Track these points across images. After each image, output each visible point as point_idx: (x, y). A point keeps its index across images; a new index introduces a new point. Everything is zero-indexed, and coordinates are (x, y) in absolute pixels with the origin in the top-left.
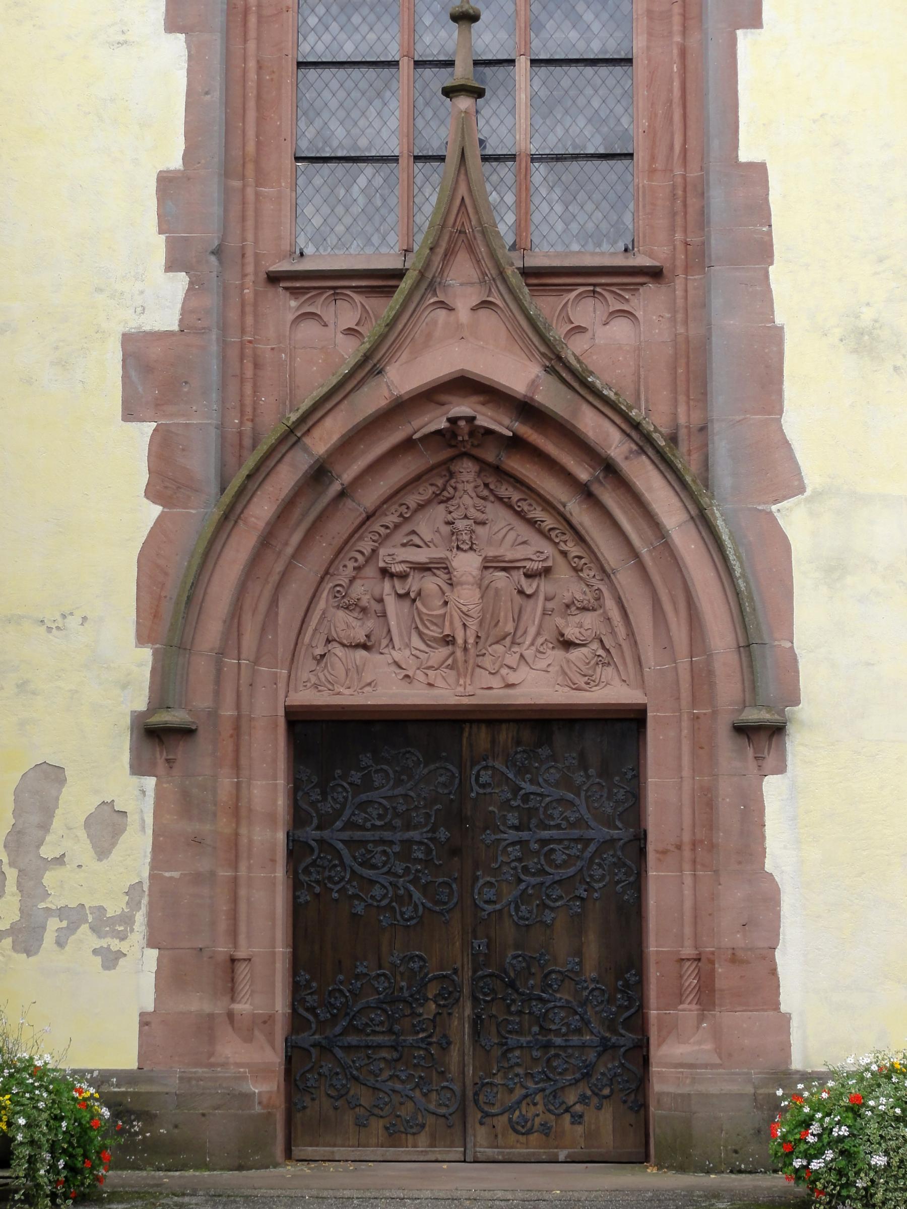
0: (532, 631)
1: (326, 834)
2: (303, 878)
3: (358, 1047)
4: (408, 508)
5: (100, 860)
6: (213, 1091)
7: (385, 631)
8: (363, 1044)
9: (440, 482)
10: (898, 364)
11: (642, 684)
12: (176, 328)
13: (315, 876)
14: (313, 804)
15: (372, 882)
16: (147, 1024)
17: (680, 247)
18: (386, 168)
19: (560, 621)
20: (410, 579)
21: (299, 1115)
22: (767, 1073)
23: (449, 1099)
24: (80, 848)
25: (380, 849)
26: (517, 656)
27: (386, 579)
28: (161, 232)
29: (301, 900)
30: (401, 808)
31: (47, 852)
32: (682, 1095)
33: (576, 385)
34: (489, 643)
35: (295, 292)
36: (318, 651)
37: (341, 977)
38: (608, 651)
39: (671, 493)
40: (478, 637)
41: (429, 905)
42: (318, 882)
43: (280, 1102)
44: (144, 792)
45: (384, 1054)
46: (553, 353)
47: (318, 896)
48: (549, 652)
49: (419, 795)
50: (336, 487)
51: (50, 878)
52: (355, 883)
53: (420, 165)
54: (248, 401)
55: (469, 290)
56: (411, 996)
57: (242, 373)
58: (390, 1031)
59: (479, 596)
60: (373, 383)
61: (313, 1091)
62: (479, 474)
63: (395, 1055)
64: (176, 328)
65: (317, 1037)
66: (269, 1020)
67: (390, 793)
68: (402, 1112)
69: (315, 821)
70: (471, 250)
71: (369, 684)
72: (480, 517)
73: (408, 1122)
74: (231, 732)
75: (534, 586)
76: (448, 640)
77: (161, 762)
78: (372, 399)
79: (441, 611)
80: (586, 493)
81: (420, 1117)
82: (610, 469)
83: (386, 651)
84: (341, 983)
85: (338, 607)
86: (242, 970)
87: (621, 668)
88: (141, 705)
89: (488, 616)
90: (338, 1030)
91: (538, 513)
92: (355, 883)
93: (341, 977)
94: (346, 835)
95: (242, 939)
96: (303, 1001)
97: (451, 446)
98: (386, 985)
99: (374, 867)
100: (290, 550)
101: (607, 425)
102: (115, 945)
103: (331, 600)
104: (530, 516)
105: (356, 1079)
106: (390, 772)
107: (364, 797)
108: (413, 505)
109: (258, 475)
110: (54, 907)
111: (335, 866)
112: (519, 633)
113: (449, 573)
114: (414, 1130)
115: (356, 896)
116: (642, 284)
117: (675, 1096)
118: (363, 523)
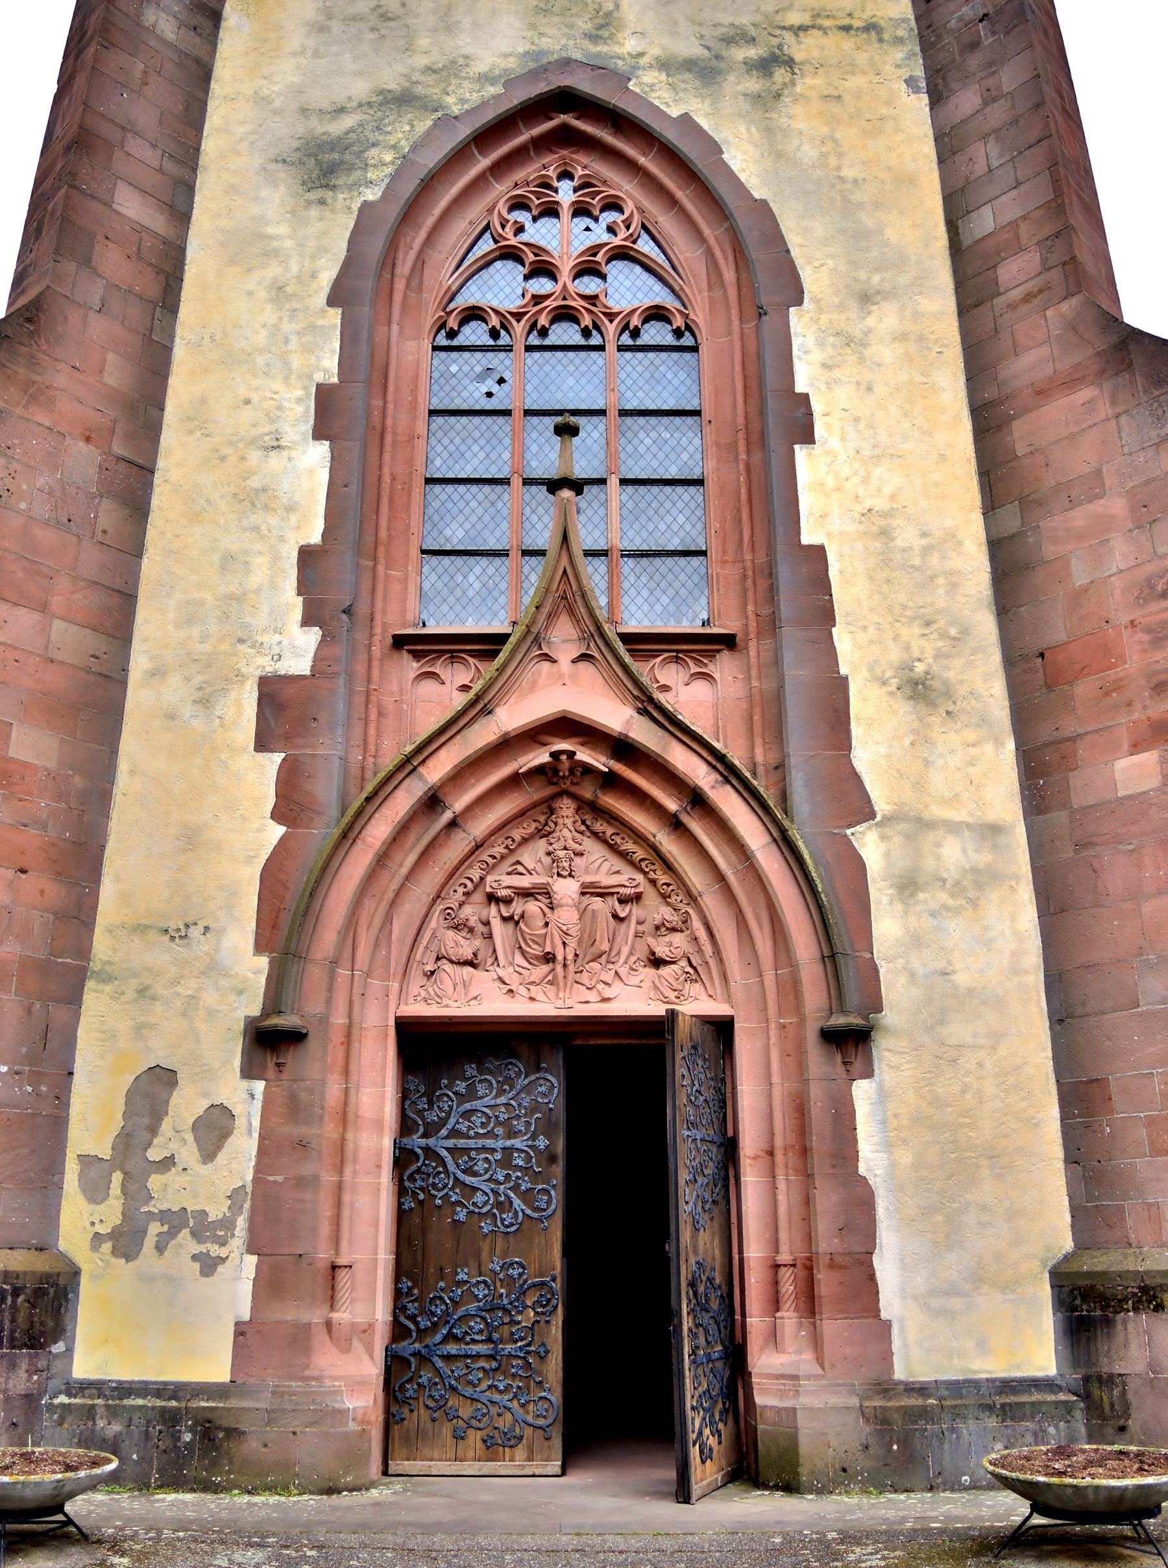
0: (625, 950)
1: (431, 1142)
2: (407, 1184)
3: (456, 1357)
4: (513, 841)
5: (205, 1163)
6: (306, 1407)
7: (491, 951)
8: (462, 1353)
9: (542, 819)
10: (950, 709)
11: (729, 999)
12: (308, 673)
13: (419, 1183)
14: (420, 1113)
15: (475, 1189)
16: (242, 1334)
17: (751, 616)
18: (497, 561)
19: (651, 941)
20: (515, 902)
21: (396, 1427)
22: (870, 1384)
23: (547, 1411)
24: (188, 1153)
25: (483, 1156)
26: (613, 972)
27: (493, 904)
28: (299, 594)
29: (406, 1207)
30: (503, 1117)
31: (154, 1155)
32: (785, 1409)
33: (666, 724)
34: (588, 958)
35: (417, 655)
36: (429, 968)
37: (442, 1284)
38: (695, 969)
39: (754, 818)
40: (576, 955)
41: (528, 1212)
42: (422, 1189)
43: (377, 1416)
44: (252, 1096)
45: (482, 1363)
46: (647, 696)
47: (421, 1203)
48: (641, 969)
49: (520, 1105)
50: (448, 816)
51: (155, 1182)
52: (457, 1190)
53: (527, 558)
54: (372, 740)
55: (570, 646)
56: (510, 1303)
57: (367, 716)
58: (489, 1340)
59: (577, 917)
60: (483, 721)
61: (411, 1402)
62: (577, 811)
63: (494, 1364)
64: (308, 673)
65: (417, 1345)
66: (369, 1329)
67: (493, 1102)
68: (500, 1423)
69: (421, 1129)
70: (572, 612)
71: (475, 998)
72: (578, 848)
73: (505, 1434)
74: (343, 1039)
75: (627, 910)
76: (549, 958)
77: (271, 1065)
78: (483, 735)
79: (544, 931)
80: (675, 824)
81: (517, 1430)
82: (697, 800)
83: (491, 968)
84: (442, 1290)
85: (448, 928)
86: (343, 1276)
87: (707, 985)
88: (255, 1010)
89: (586, 936)
90: (438, 1338)
91: (629, 846)
92: (457, 1190)
93: (442, 1284)
94: (450, 1143)
95: (344, 1244)
96: (404, 1308)
97: (553, 784)
98: (486, 1292)
99: (475, 1174)
100: (404, 870)
101: (695, 759)
102: (215, 1250)
103: (442, 921)
104: (623, 848)
105: (453, 1389)
106: (494, 1082)
107: (468, 1106)
108: (518, 838)
109: (376, 797)
110: (156, 1211)
111: (440, 1173)
112: (614, 953)
113: (550, 898)
114: (512, 1442)
115: (459, 1203)
116: (718, 651)
117: (778, 1410)
118: (472, 853)
